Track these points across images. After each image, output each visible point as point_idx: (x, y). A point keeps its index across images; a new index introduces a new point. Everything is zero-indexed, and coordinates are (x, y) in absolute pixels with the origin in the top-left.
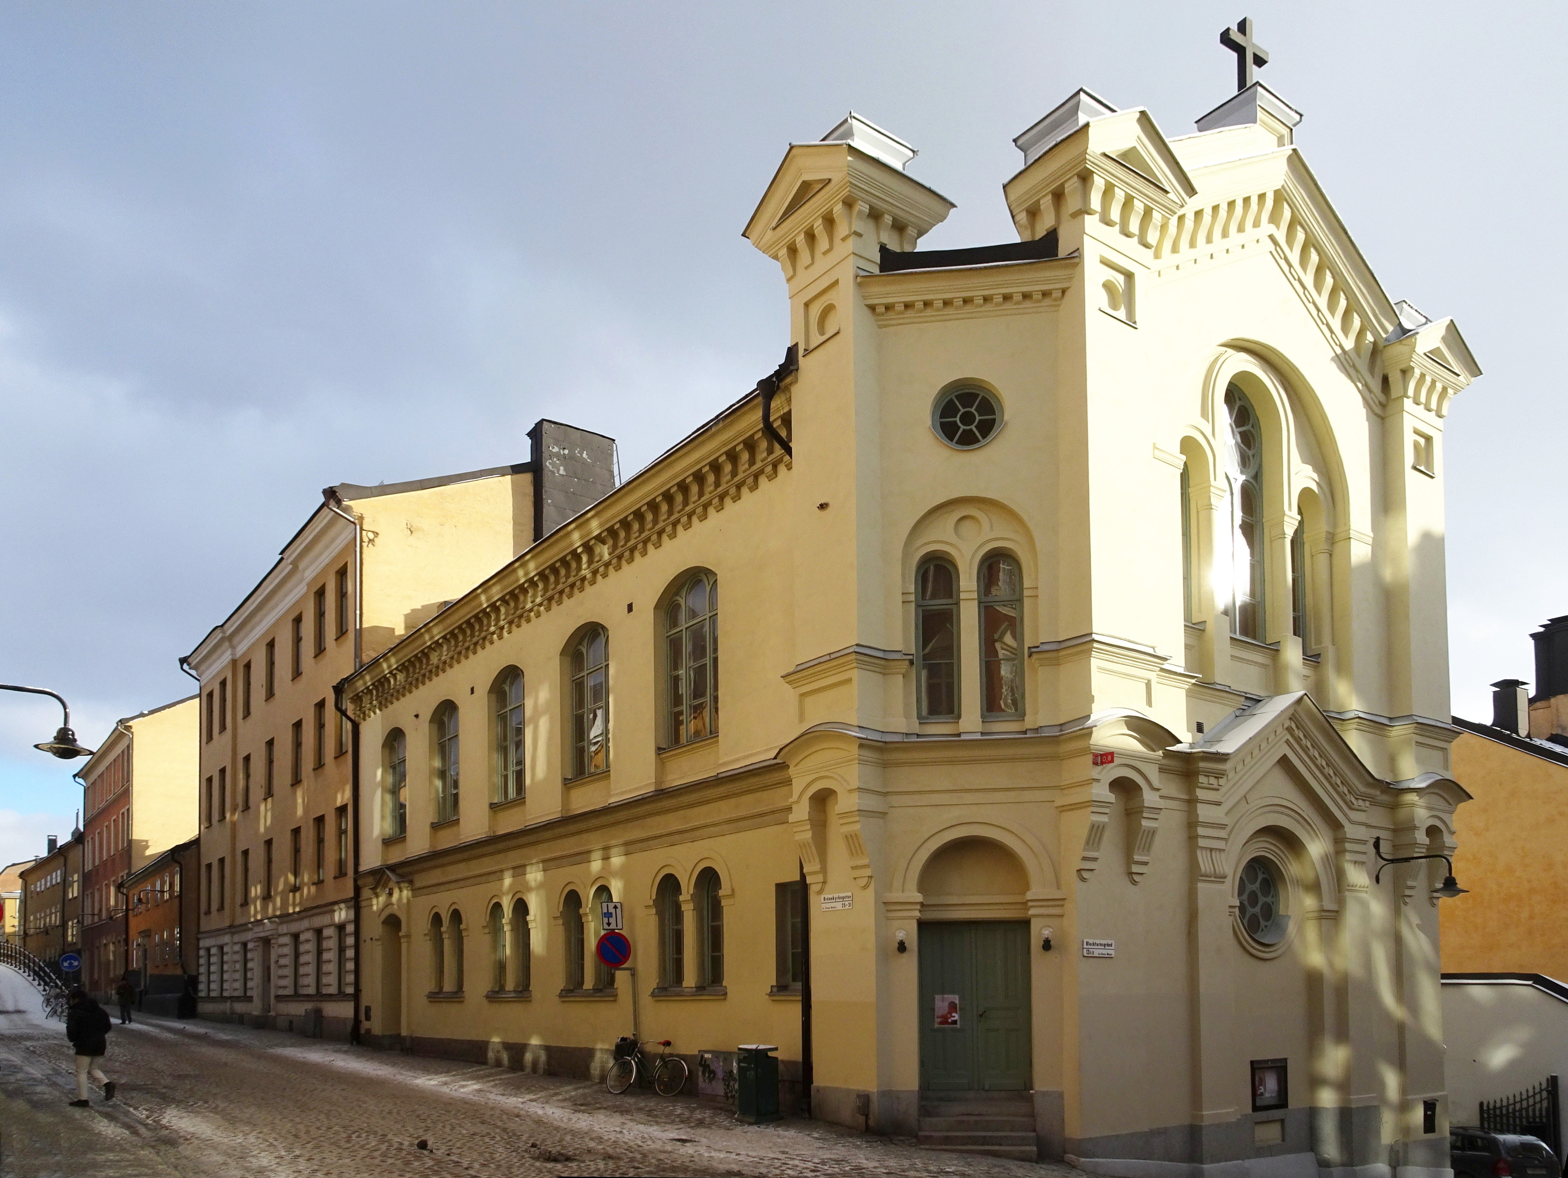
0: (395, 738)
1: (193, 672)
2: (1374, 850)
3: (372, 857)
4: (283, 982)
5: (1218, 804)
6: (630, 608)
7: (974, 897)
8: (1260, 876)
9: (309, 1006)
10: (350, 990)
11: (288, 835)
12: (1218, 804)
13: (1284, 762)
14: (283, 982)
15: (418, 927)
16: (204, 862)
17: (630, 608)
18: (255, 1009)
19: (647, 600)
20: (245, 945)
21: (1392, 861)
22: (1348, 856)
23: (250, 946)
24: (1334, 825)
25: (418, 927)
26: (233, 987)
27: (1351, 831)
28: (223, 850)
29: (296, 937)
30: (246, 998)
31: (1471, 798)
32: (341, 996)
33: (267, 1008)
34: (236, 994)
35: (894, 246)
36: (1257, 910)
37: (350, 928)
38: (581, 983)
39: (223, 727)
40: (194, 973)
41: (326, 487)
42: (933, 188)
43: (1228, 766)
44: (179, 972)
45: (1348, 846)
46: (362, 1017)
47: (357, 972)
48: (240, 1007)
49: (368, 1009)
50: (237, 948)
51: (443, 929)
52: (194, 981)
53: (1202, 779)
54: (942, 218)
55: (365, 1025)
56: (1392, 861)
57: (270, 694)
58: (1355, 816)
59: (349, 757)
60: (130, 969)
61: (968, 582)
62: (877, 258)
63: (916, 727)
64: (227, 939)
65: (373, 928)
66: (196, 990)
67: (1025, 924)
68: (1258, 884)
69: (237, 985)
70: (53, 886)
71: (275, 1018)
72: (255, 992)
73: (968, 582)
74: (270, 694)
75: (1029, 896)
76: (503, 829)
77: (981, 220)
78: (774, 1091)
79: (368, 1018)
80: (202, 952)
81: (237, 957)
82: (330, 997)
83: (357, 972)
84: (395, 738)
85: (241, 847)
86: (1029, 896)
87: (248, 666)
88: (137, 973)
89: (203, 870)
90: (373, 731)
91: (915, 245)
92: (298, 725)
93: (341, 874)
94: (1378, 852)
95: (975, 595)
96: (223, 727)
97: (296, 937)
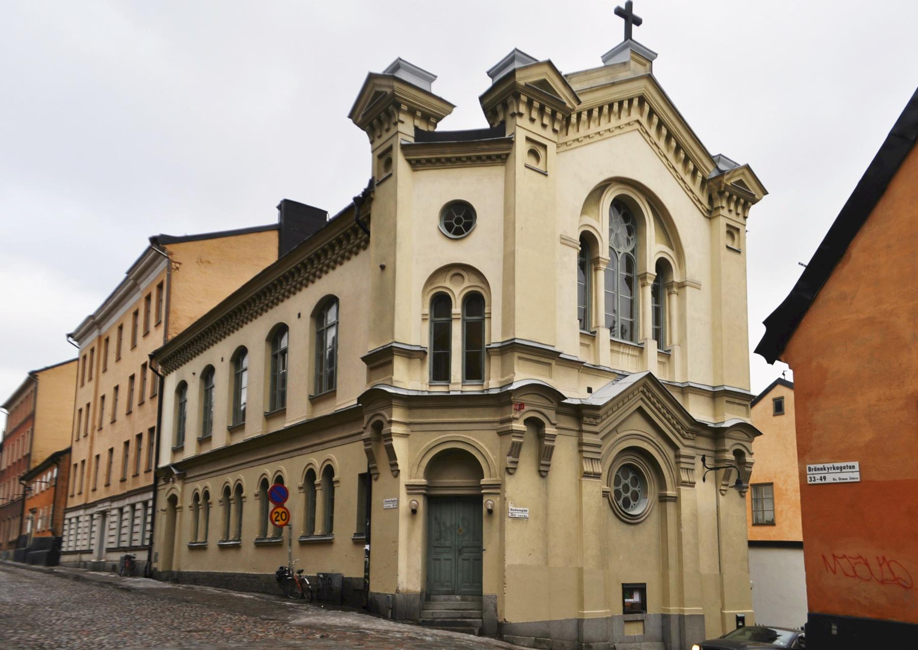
0: (182, 388)
1: (75, 343)
2: (701, 463)
3: (166, 460)
4: (112, 539)
5: (596, 433)
6: (299, 316)
7: (454, 481)
8: (631, 475)
9: (123, 554)
10: (147, 543)
11: (122, 445)
12: (596, 433)
13: (640, 410)
14: (112, 539)
15: (186, 502)
16: (73, 462)
17: (299, 316)
18: (93, 558)
19: (307, 311)
20: (92, 515)
21: (711, 469)
22: (682, 465)
23: (95, 516)
24: (675, 448)
25: (186, 502)
26: (82, 545)
27: (684, 451)
28: (84, 456)
29: (121, 510)
30: (90, 552)
31: (760, 434)
32: (141, 548)
33: (100, 557)
34: (84, 548)
35: (423, 127)
36: (629, 494)
37: (150, 504)
38: (266, 534)
39: (90, 379)
40: (60, 536)
41: (278, 203)
42: (444, 97)
43: (601, 412)
44: (49, 535)
45: (682, 460)
46: (153, 559)
47: (152, 531)
48: (85, 557)
49: (157, 554)
50: (88, 518)
51: (200, 503)
52: (59, 541)
53: (585, 419)
54: (450, 113)
55: (155, 565)
56: (711, 469)
57: (118, 359)
58: (687, 442)
59: (157, 398)
60: (24, 533)
61: (457, 309)
62: (412, 133)
63: (425, 387)
64: (81, 512)
65: (163, 503)
66: (60, 547)
67: (480, 497)
68: (629, 480)
69: (85, 542)
70: (42, 492)
71: (104, 563)
72: (95, 548)
73: (457, 309)
74: (118, 359)
75: (483, 482)
76: (234, 443)
77: (468, 117)
78: (352, 595)
79: (156, 561)
80: (66, 522)
81: (87, 524)
82: (136, 549)
83: (152, 531)
84: (182, 388)
85: (95, 453)
86: (483, 482)
87: (107, 340)
88: (26, 537)
89: (72, 468)
90: (171, 383)
91: (435, 126)
92: (132, 378)
93: (148, 471)
94: (704, 464)
95: (460, 316)
96: (90, 379)
97: (121, 510)
